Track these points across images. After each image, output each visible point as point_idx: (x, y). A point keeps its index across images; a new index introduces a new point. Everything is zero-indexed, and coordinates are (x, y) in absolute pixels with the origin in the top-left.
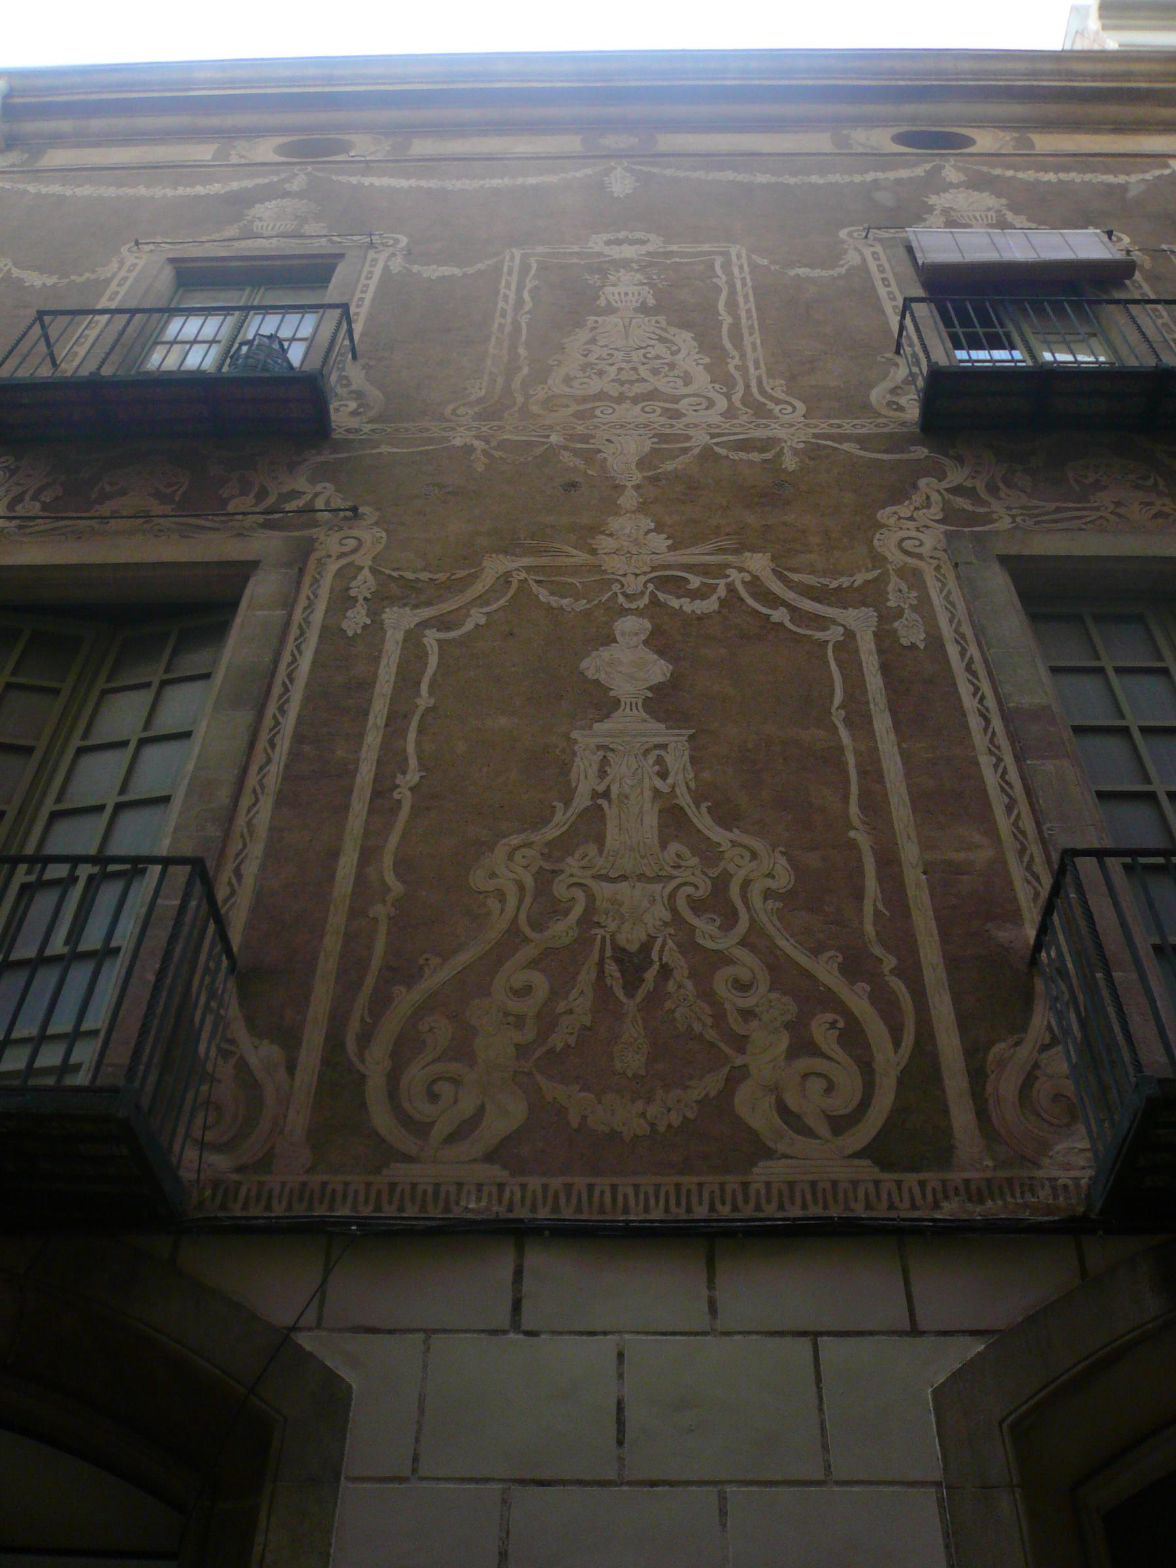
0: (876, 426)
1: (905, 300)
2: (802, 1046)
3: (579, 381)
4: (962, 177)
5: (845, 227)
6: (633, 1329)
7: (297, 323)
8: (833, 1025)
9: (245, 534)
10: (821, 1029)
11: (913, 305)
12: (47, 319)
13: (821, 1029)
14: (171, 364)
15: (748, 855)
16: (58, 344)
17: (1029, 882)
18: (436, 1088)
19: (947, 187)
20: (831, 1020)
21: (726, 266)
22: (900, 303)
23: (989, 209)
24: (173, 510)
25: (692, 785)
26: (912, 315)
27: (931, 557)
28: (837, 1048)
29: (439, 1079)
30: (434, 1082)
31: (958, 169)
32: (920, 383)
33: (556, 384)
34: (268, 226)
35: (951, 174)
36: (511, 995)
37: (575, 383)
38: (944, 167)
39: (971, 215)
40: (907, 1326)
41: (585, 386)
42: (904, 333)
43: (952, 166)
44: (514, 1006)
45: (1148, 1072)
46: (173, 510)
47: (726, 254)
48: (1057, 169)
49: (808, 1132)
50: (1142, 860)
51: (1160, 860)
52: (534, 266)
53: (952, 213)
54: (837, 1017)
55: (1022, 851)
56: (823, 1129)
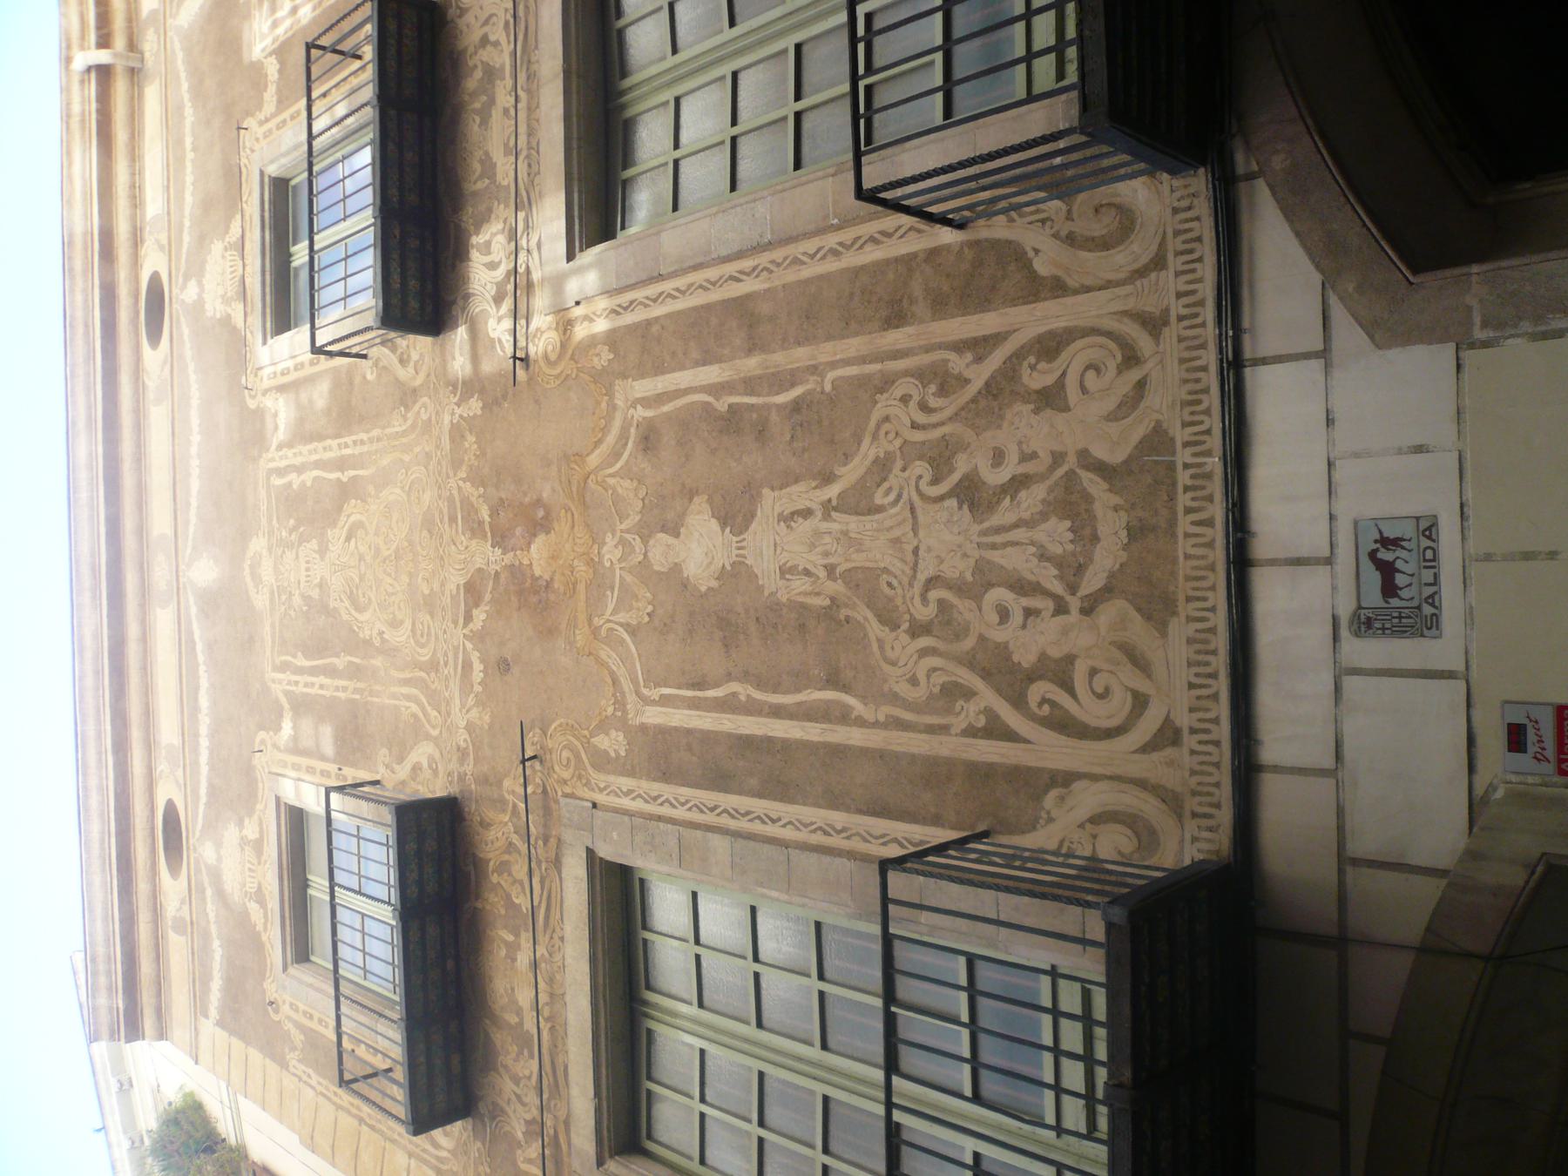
0: (446, 666)
2: (1051, 398)
4: (192, 284)
5: (245, 402)
6: (1383, 253)
8: (1033, 367)
9: (552, 1132)
10: (1037, 378)
11: (318, 345)
12: (347, 1076)
13: (1037, 378)
14: (386, 971)
16: (317, 83)
18: (1100, 690)
19: (200, 303)
20: (1029, 371)
21: (281, 472)
24: (527, 931)
25: (788, 565)
30: (1094, 692)
31: (184, 287)
32: (392, 335)
33: (400, 637)
34: (250, 876)
35: (191, 293)
36: (1002, 627)
42: (347, 351)
44: (1017, 618)
45: (1076, 123)
47: (271, 472)
48: (180, 193)
49: (1141, 385)
50: (862, 110)
51: (862, 122)
52: (283, 658)
56: (1134, 375)
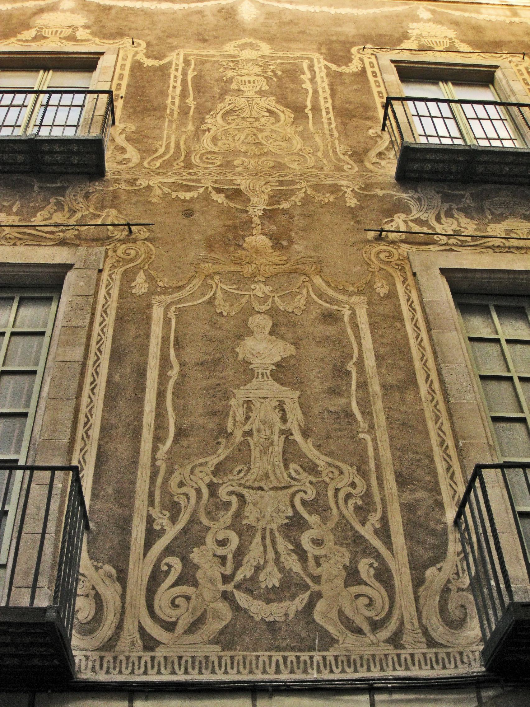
1: (387, 98)
3: (222, 141)
7: (98, 104)
8: (371, 565)
11: (393, 102)
15: (337, 472)
17: (445, 460)
18: (177, 602)
22: (384, 100)
23: (446, 37)
24: (20, 221)
26: (392, 108)
27: (396, 264)
28: (374, 581)
29: (177, 597)
37: (220, 143)
38: (418, 8)
39: (441, 41)
40: (80, 108)
41: (227, 146)
43: (424, 8)
46: (20, 221)
47: (311, 60)
49: (359, 631)
53: (422, 39)
54: (374, 561)
55: (442, 443)
56: (366, 628)
